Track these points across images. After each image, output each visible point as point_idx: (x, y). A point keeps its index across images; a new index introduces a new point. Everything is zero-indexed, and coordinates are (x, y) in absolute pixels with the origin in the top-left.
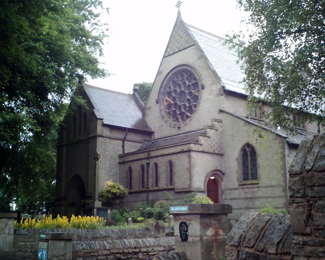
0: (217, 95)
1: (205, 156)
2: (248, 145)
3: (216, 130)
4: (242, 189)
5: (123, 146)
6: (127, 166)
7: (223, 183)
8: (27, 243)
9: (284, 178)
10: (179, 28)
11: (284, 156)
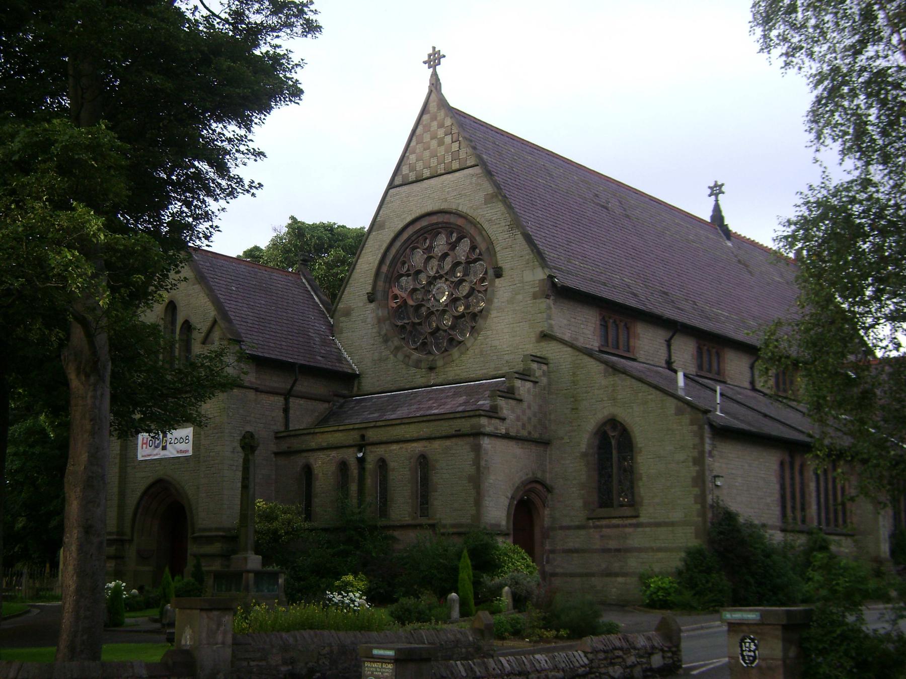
0: (535, 296)
1: (515, 449)
2: (613, 422)
3: (535, 383)
4: (596, 527)
5: (286, 410)
6: (300, 460)
7: (547, 512)
8: (252, 663)
9: (699, 506)
10: (434, 118)
11: (702, 453)
